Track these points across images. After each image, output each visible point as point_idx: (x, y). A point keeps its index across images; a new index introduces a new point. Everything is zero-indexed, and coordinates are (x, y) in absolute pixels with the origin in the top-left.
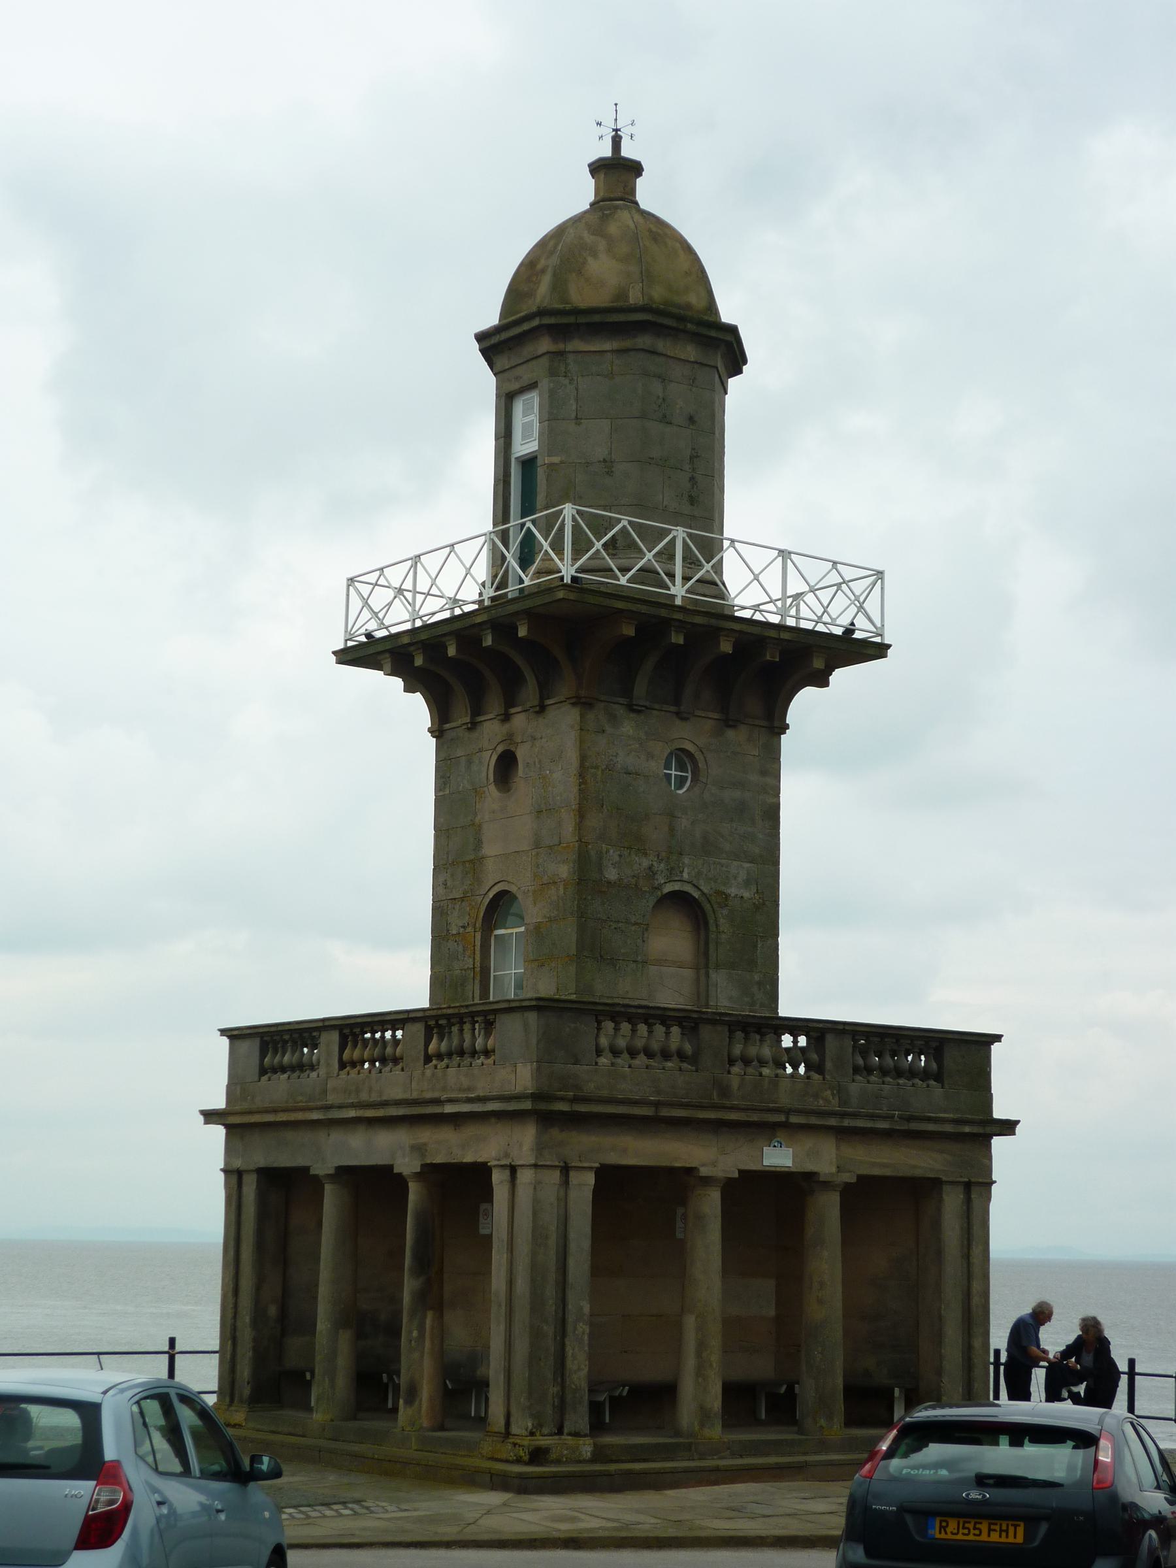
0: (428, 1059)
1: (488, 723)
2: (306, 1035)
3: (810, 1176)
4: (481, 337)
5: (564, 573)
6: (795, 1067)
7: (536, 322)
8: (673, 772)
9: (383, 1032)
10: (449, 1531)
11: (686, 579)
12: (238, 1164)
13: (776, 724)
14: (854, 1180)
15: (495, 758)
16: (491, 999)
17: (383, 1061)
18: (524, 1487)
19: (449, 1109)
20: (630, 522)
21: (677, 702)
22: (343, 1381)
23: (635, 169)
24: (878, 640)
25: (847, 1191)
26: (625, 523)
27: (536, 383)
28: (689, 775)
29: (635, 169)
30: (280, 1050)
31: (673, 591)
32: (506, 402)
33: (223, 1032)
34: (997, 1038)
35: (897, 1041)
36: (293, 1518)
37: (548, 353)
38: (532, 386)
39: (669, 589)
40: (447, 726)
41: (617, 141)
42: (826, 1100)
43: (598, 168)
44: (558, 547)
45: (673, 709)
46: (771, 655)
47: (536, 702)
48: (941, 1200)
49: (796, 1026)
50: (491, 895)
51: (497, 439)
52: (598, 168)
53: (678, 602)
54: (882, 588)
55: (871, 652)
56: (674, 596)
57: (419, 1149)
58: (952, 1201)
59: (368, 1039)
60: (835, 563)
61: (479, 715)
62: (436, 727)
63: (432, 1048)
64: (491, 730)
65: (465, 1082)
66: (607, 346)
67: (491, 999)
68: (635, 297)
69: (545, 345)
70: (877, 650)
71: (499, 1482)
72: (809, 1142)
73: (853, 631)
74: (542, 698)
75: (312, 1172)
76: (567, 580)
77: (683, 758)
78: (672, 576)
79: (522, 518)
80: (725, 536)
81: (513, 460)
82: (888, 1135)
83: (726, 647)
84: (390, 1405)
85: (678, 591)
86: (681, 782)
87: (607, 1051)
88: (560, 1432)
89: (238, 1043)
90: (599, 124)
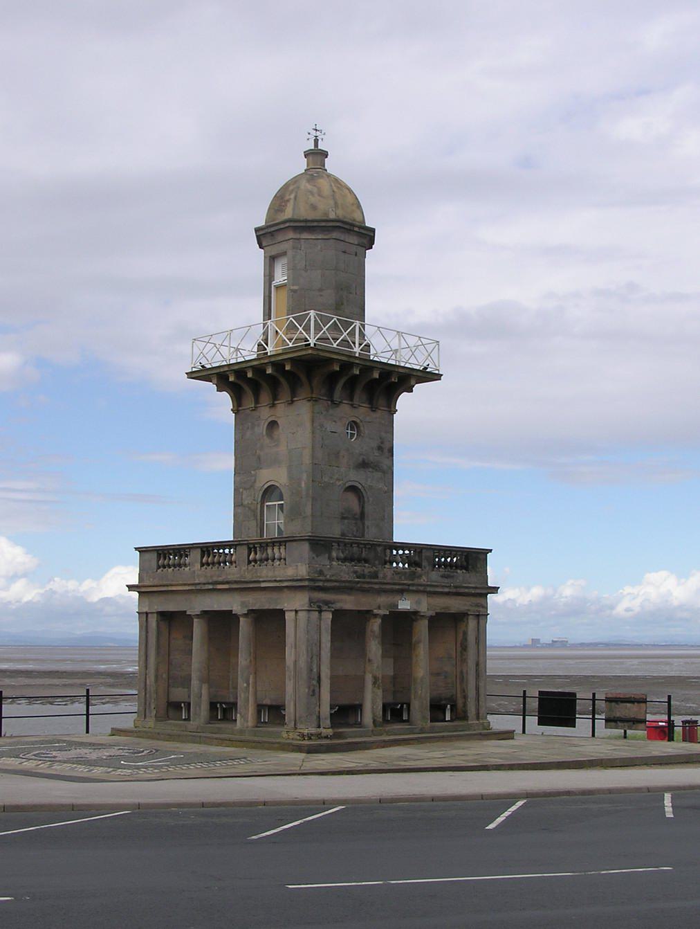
0: (249, 562)
1: (263, 408)
2: (210, 549)
3: (416, 613)
4: (257, 230)
5: (310, 342)
6: (397, 564)
7: (287, 225)
8: (349, 431)
9: (224, 550)
10: (283, 769)
11: (360, 345)
12: (145, 610)
13: (393, 409)
14: (434, 614)
15: (267, 424)
16: (265, 537)
17: (231, 563)
18: (311, 750)
19: (263, 585)
20: (337, 319)
21: (352, 400)
22: (205, 707)
23: (325, 154)
24: (437, 372)
25: (432, 620)
26: (335, 319)
27: (286, 252)
28: (356, 432)
29: (325, 154)
30: (162, 558)
31: (355, 350)
32: (271, 261)
33: (136, 549)
34: (491, 551)
35: (351, 546)
36: (222, 766)
37: (292, 239)
38: (284, 254)
39: (353, 349)
40: (240, 408)
41: (316, 141)
42: (424, 580)
43: (307, 154)
44: (307, 329)
45: (350, 403)
46: (394, 379)
47: (290, 399)
48: (468, 622)
49: (403, 546)
50: (266, 486)
51: (264, 276)
52: (307, 154)
53: (357, 355)
54: (439, 349)
55: (436, 378)
56: (355, 352)
57: (243, 604)
58: (472, 623)
59: (216, 553)
60: (379, 328)
61: (258, 404)
62: (235, 408)
63: (252, 557)
64: (265, 414)
65: (270, 574)
66: (320, 236)
67: (265, 537)
68: (332, 216)
69: (291, 235)
70: (437, 377)
71: (299, 749)
72: (416, 597)
73: (427, 368)
74: (292, 398)
75: (188, 613)
76: (312, 345)
77: (354, 425)
78: (354, 343)
79: (288, 315)
80: (366, 322)
81: (273, 287)
82: (448, 594)
83: (376, 375)
84: (234, 718)
85: (357, 350)
86: (352, 435)
87: (335, 559)
88: (319, 727)
89: (143, 554)
90: (309, 134)
